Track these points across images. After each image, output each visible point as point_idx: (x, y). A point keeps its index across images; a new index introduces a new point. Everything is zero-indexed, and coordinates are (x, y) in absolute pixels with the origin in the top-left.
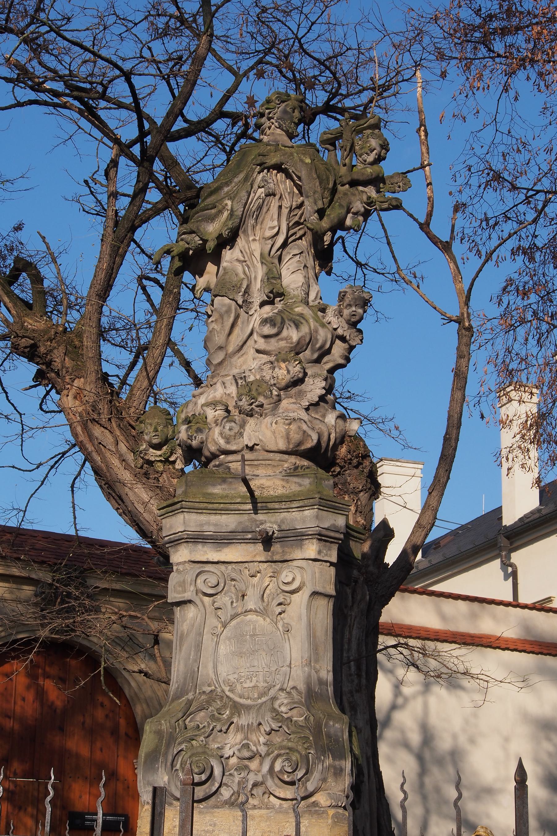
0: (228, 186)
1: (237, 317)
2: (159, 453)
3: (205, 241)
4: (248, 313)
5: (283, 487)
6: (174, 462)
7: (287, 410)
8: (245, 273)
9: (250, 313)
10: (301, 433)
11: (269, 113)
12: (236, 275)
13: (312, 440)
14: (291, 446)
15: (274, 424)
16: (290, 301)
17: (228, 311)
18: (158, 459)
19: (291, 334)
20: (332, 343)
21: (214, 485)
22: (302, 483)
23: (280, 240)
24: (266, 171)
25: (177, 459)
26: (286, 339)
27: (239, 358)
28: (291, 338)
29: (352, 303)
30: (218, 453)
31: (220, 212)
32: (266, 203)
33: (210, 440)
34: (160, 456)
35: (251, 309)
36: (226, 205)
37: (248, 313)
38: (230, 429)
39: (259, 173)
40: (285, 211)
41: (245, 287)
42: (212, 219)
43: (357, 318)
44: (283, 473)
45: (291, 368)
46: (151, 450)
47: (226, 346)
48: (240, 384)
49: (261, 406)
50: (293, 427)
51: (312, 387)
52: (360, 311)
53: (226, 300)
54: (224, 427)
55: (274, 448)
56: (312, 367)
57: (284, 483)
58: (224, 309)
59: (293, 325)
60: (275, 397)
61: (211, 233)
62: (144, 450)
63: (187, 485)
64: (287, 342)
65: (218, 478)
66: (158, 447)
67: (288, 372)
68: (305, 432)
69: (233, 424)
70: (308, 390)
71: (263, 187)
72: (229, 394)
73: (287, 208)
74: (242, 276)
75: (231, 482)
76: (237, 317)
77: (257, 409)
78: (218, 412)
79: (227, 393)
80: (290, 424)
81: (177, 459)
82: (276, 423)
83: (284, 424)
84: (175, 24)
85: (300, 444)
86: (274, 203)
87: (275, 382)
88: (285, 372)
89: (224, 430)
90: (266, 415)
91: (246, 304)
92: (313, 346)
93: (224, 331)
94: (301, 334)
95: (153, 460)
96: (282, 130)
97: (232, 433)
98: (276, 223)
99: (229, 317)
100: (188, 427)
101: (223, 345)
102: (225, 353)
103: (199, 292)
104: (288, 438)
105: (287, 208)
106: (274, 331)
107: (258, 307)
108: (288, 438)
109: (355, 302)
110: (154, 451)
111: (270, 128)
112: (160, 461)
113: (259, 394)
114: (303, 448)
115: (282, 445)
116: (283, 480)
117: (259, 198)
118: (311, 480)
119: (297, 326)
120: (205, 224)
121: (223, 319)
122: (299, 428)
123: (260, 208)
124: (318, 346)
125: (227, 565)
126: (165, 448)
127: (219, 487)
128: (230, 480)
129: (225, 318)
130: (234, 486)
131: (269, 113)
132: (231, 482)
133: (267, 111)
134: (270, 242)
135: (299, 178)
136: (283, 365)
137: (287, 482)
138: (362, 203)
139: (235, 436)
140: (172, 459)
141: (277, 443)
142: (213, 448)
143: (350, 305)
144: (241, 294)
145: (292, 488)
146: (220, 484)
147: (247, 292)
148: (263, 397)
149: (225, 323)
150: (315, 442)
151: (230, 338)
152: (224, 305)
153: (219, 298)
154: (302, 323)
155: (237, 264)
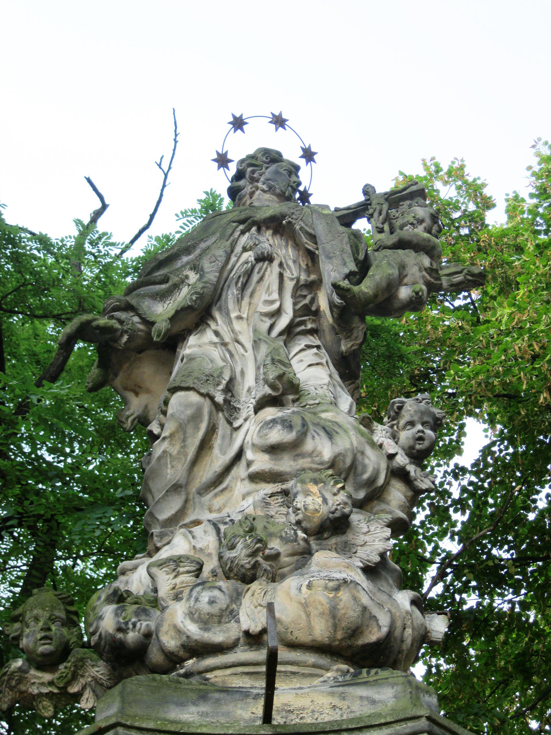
0: (189, 254)
1: (212, 430)
2: (47, 677)
3: (150, 324)
4: (230, 423)
5: (334, 707)
6: (77, 697)
7: (325, 566)
8: (224, 360)
9: (236, 425)
10: (359, 609)
11: (253, 172)
12: (212, 361)
13: (380, 627)
14: (340, 635)
15: (304, 589)
16: (312, 402)
17: (196, 417)
18: (45, 690)
19: (319, 448)
20: (387, 483)
21: (181, 704)
22: (377, 697)
23: (283, 322)
24: (254, 229)
25: (84, 688)
26: (310, 455)
27: (216, 495)
28: (320, 454)
29: (416, 418)
30: (181, 653)
31: (176, 287)
32: (256, 270)
33: (165, 628)
34: (51, 683)
35: (236, 418)
36: (187, 277)
37: (230, 423)
38: (212, 602)
39: (243, 233)
40: (289, 285)
41: (227, 378)
42: (162, 296)
43: (426, 444)
44: (332, 683)
45: (328, 496)
46: (33, 672)
47: (187, 484)
48: (222, 530)
49: (276, 557)
50: (344, 595)
51: (367, 538)
52: (429, 432)
53: (193, 397)
54: (197, 600)
55: (303, 637)
56: (357, 513)
57: (336, 701)
58: (189, 412)
59: (322, 433)
60: (302, 543)
61: (160, 315)
62: (20, 669)
63: (123, 701)
64: (313, 462)
65: (191, 690)
66: (46, 663)
67: (325, 501)
68: (365, 609)
69: (216, 593)
70: (360, 541)
71: (251, 249)
72: (201, 550)
73: (292, 279)
74: (221, 364)
75: (217, 701)
76: (212, 430)
77: (265, 565)
78: (182, 578)
79: (198, 546)
80: (337, 589)
81: (84, 688)
82: (309, 586)
83: (326, 588)
84: (13, 560)
85: (355, 631)
86: (272, 273)
87: (300, 517)
88: (320, 500)
89: (198, 605)
90: (283, 577)
91: (228, 408)
92: (356, 475)
93: (186, 455)
94: (337, 450)
95: (36, 691)
96: (274, 194)
97: (215, 610)
98: (275, 296)
99: (197, 428)
100: (117, 609)
101: (183, 481)
102: (183, 497)
103: (130, 420)
104: (334, 617)
105: (292, 279)
106: (289, 437)
107: (252, 412)
108: (333, 613)
109: (421, 418)
110: (40, 674)
111: (252, 194)
112: (50, 695)
113: (271, 535)
114: (360, 642)
115: (320, 630)
116: (332, 694)
117: (247, 262)
118: (399, 688)
119: (330, 435)
120: (152, 302)
121: (185, 433)
122: (355, 599)
123: (249, 274)
124: (366, 476)
125: (399, 718)
126: (61, 667)
127: (193, 709)
128: (217, 695)
129: (190, 430)
130: (225, 709)
131: (253, 172)
132: (217, 701)
133: (249, 169)
134: (268, 322)
135: (313, 238)
136: (314, 489)
137: (343, 697)
138: (420, 270)
139: (221, 616)
140: (74, 689)
141: (310, 627)
142: (170, 642)
143: (412, 424)
144: (221, 387)
145: (354, 708)
146: (194, 704)
147: (229, 389)
148: (278, 541)
149: (189, 441)
150: (385, 630)
151: (196, 469)
152: (188, 405)
153: (180, 394)
154: (337, 433)
155: (212, 348)
